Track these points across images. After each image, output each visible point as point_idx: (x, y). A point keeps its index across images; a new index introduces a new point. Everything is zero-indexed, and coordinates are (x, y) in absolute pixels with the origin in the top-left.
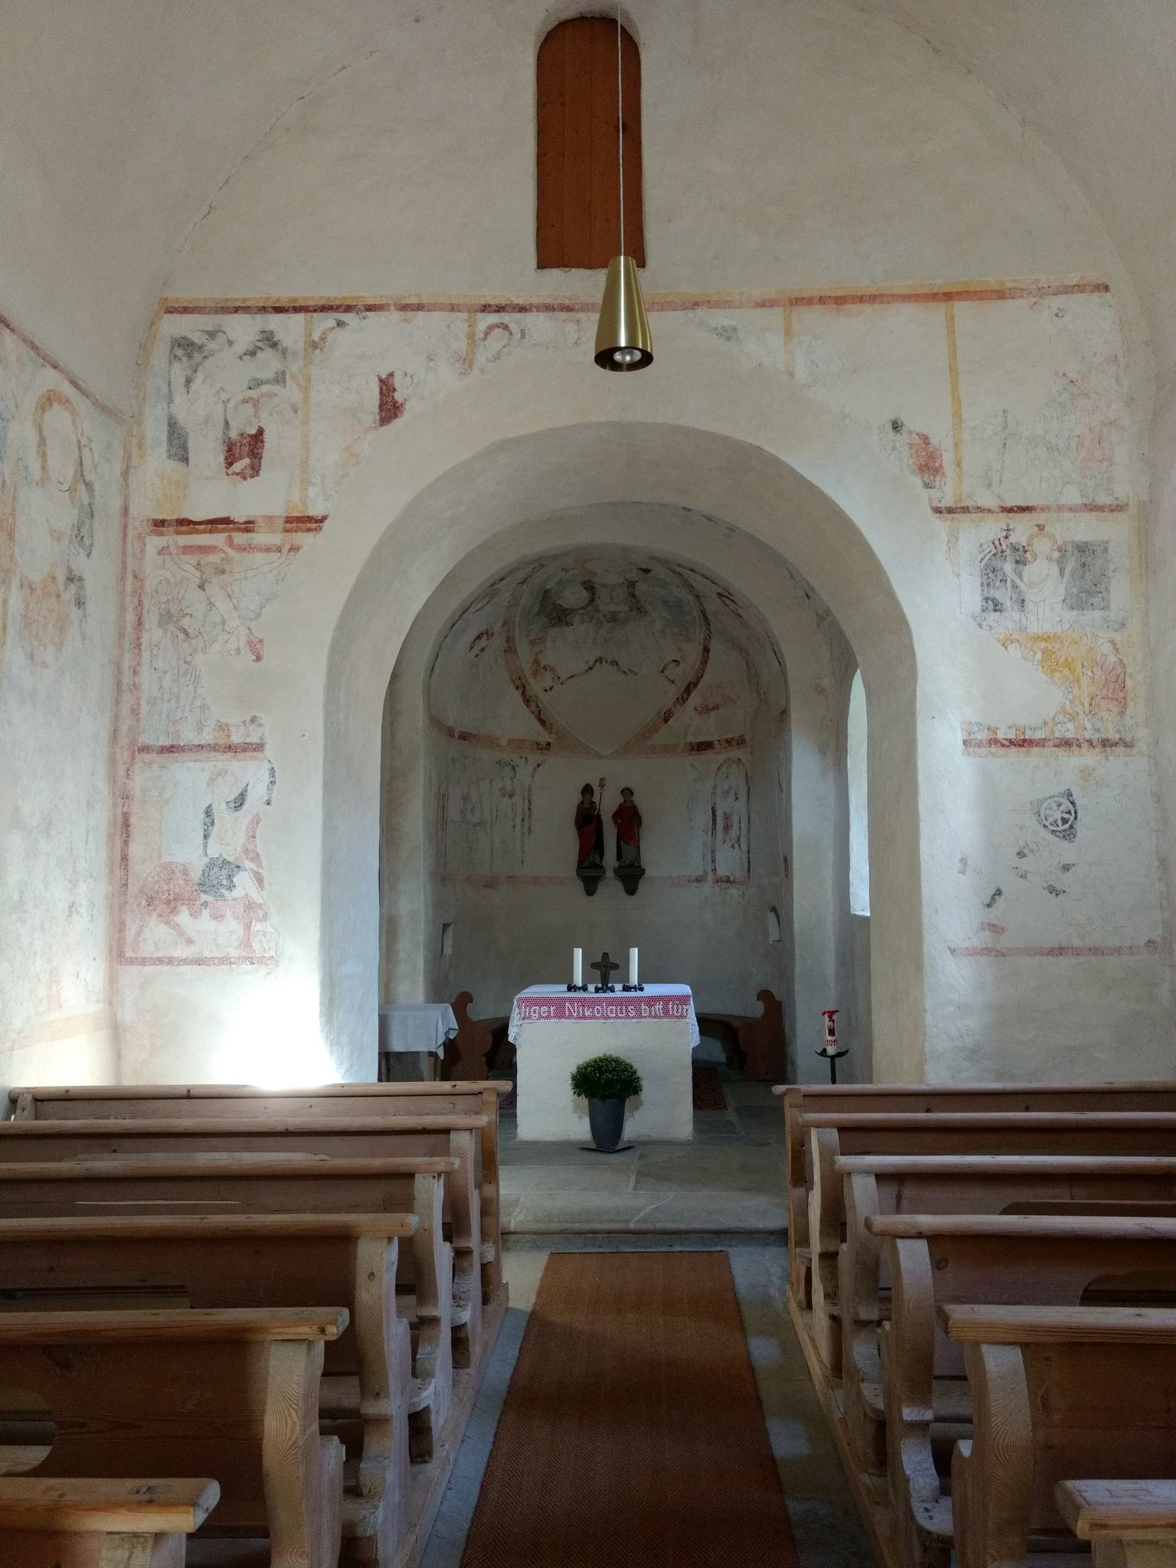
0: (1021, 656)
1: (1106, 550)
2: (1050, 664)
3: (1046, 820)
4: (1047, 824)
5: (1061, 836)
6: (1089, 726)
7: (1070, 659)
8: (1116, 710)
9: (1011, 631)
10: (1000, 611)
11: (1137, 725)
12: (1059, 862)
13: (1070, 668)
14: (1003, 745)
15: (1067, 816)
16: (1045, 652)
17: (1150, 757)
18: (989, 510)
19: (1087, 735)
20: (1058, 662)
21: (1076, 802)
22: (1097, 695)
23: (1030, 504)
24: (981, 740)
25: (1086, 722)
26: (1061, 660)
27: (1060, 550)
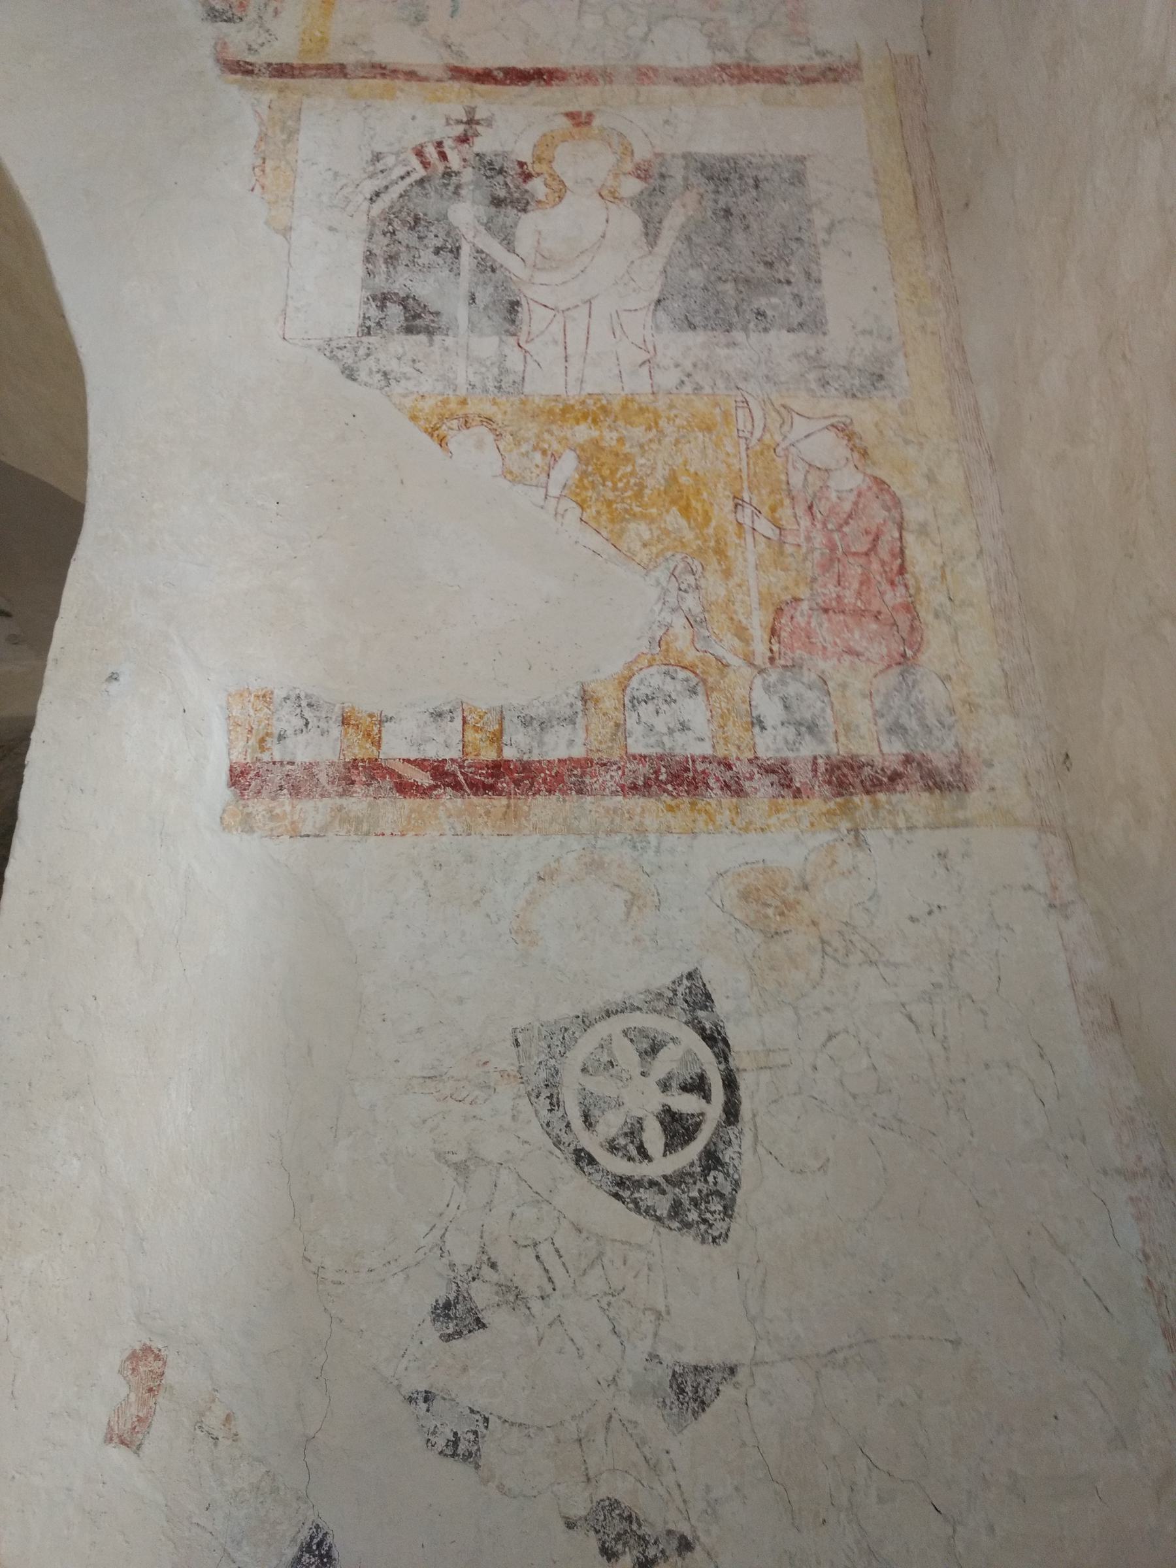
0: (497, 468)
1: (798, 179)
2: (610, 495)
3: (588, 1121)
4: (591, 1143)
5: (663, 1206)
6: (771, 710)
7: (684, 479)
8: (878, 650)
9: (462, 392)
10: (430, 332)
11: (972, 707)
12: (653, 1357)
13: (686, 511)
14: (404, 787)
15: (687, 1104)
16: (590, 455)
17: (1044, 827)
18: (411, 75)
19: (768, 747)
20: (641, 487)
21: (732, 1033)
22: (797, 600)
23: (546, 63)
24: (309, 768)
25: (758, 695)
26: (650, 482)
27: (642, 173)
